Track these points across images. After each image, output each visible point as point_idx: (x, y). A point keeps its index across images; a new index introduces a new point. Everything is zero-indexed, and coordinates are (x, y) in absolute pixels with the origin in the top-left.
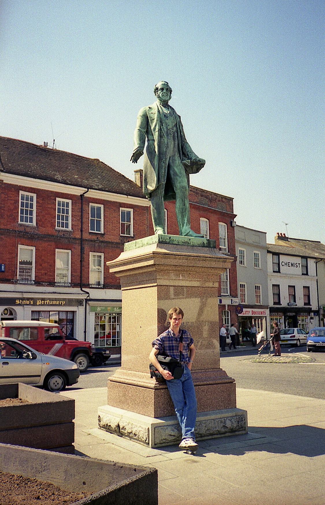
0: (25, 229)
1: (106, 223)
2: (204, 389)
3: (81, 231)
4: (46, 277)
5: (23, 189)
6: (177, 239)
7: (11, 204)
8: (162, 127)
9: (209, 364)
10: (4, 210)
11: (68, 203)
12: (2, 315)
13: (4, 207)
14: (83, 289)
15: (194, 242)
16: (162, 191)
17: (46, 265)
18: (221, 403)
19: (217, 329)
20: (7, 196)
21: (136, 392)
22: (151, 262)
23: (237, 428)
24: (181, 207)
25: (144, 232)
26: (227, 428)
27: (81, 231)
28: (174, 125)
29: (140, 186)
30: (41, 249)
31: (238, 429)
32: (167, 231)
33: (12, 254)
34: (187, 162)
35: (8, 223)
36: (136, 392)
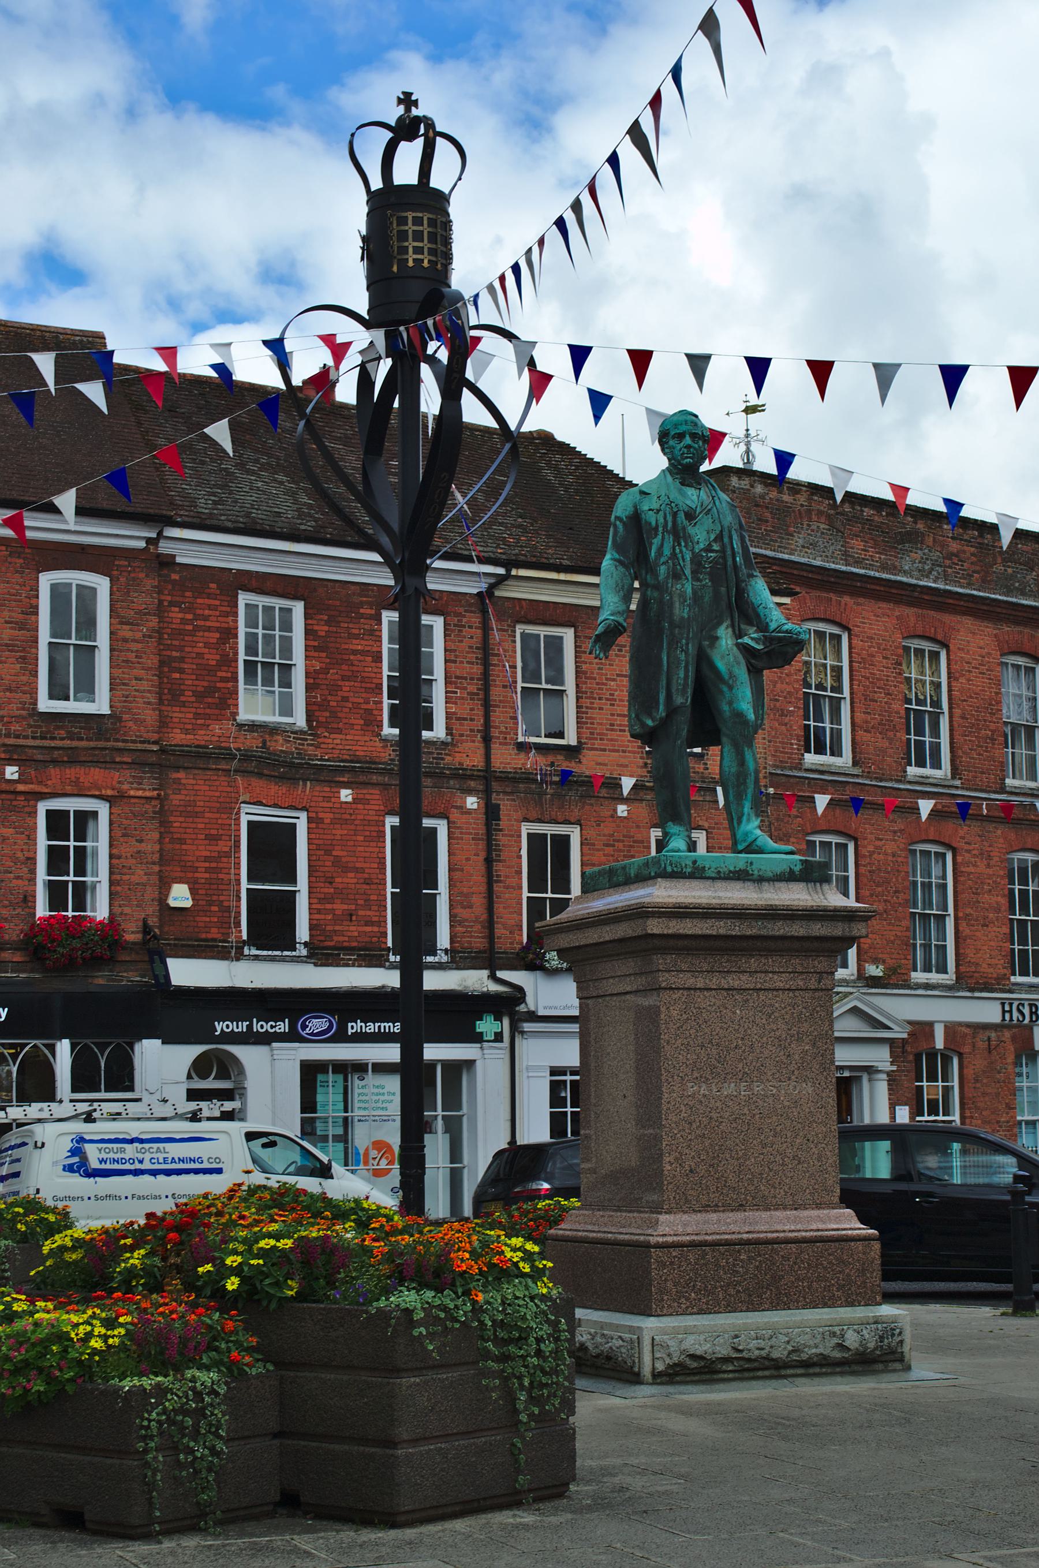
0: (264, 742)
1: (585, 702)
2: (790, 1254)
3: (487, 740)
4: (354, 930)
5: (254, 584)
6: (714, 865)
7: (207, 645)
8: (678, 550)
9: (808, 1191)
10: (181, 671)
12: (189, 1077)
13: (182, 659)
14: (501, 974)
15: (763, 868)
16: (683, 727)
17: (351, 878)
20: (190, 616)
23: (878, 1352)
26: (849, 1349)
27: (487, 740)
28: (713, 537)
30: (327, 817)
31: (879, 1356)
32: (852, 717)
34: (751, 638)
35: (199, 722)
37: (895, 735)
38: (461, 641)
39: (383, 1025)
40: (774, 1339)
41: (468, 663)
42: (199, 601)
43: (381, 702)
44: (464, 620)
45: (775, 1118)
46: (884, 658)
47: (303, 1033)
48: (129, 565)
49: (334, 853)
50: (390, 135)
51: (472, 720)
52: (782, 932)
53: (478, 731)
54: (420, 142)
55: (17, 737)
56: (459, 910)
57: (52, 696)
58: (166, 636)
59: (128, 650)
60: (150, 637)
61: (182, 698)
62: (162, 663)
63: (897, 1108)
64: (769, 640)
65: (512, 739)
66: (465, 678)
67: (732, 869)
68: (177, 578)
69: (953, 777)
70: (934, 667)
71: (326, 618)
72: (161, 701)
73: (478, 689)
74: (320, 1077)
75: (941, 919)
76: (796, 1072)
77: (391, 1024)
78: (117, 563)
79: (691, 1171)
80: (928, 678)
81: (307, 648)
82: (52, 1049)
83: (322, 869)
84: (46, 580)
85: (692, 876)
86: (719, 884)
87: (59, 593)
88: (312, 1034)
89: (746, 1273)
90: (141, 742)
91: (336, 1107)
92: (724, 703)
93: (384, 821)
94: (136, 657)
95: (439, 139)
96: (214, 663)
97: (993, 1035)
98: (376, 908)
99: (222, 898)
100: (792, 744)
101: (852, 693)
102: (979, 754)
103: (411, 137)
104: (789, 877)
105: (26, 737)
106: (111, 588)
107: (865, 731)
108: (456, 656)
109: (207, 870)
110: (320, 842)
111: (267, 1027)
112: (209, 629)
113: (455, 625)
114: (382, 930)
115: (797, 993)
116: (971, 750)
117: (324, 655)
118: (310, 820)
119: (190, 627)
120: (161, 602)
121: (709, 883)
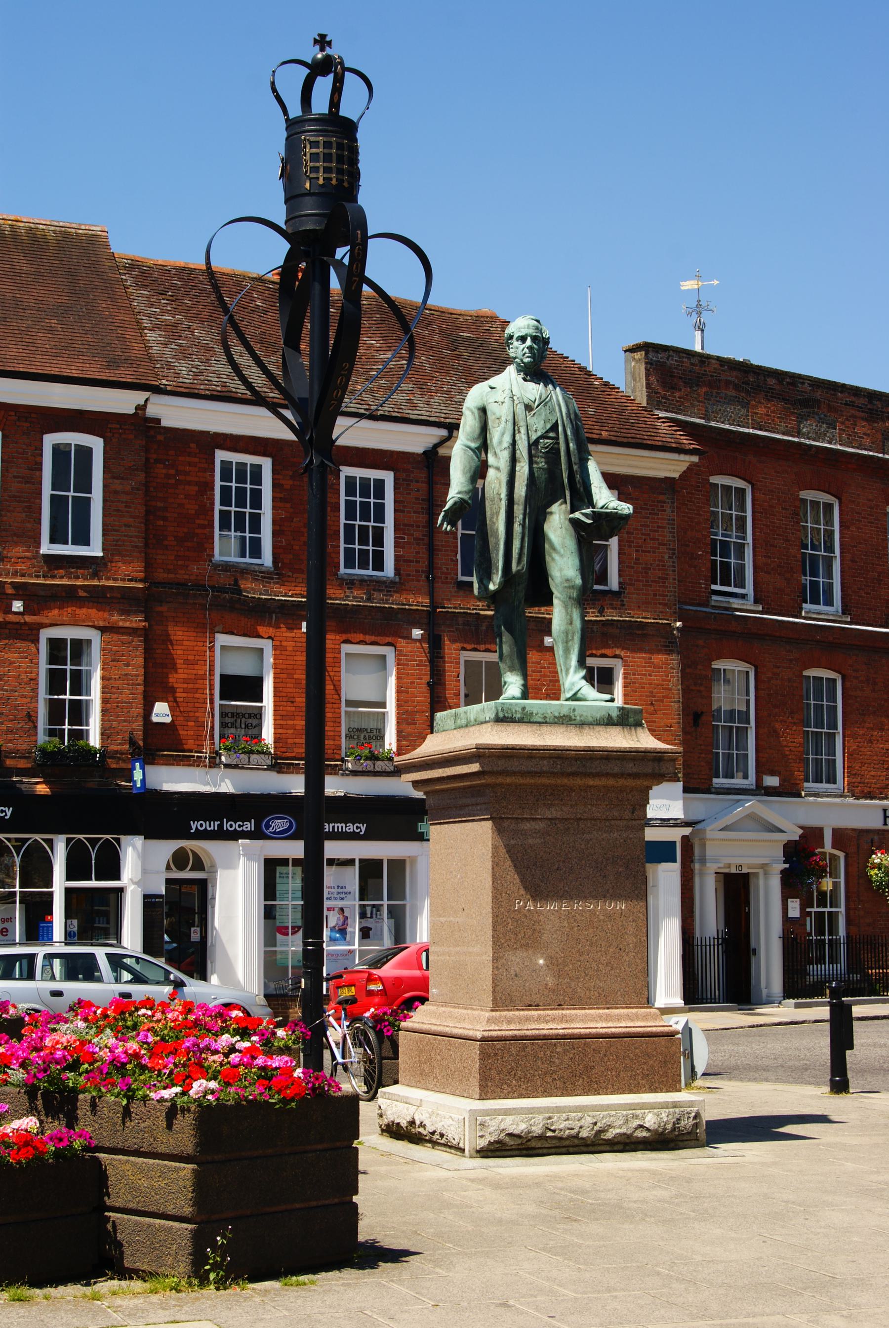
0: (236, 581)
6: (541, 712)
9: (619, 993)
10: (165, 519)
11: (380, 484)
12: (168, 868)
15: (585, 714)
18: (643, 1079)
19: (641, 915)
20: (172, 472)
21: (449, 1050)
22: (475, 767)
24: (563, 628)
25: (660, 574)
29: (645, 404)
33: (197, 667)
35: (180, 563)
36: (449, 1050)
37: (792, 576)
38: (409, 494)
39: (336, 825)
40: (583, 1121)
41: (415, 512)
42: (181, 458)
43: (339, 546)
44: (412, 475)
45: (591, 930)
46: (783, 509)
47: (267, 832)
48: (121, 428)
49: (296, 676)
50: (306, 71)
51: (417, 562)
52: (598, 770)
53: (423, 571)
54: (331, 77)
55: (23, 575)
56: (404, 726)
57: (53, 540)
58: (152, 489)
59: (119, 501)
60: (138, 489)
61: (166, 543)
62: (148, 512)
63: (789, 900)
64: (596, 516)
65: (452, 578)
66: (412, 526)
67: (557, 714)
68: (162, 439)
69: (843, 613)
70: (828, 518)
71: (291, 473)
72: (146, 545)
73: (423, 535)
74: (279, 869)
75: (831, 737)
76: (611, 891)
77: (343, 825)
78: (110, 426)
79: (516, 975)
80: (822, 527)
81: (274, 499)
82: (50, 842)
83: (284, 690)
84: (50, 440)
85: (520, 721)
86: (545, 729)
87: (60, 452)
88: (274, 833)
89: (561, 1063)
90: (130, 580)
91: (294, 896)
92: (556, 571)
93: (340, 649)
94: (126, 507)
95: (347, 74)
96: (193, 512)
97: (876, 838)
98: (332, 724)
99: (197, 714)
100: (701, 584)
101: (754, 540)
102: (867, 593)
103: (325, 74)
104: (608, 722)
105: (30, 576)
106: (105, 447)
107: (765, 573)
108: (404, 507)
109: (185, 691)
110: (284, 667)
111: (236, 826)
112: (189, 483)
113: (403, 480)
114: (336, 743)
115: (613, 822)
116: (860, 589)
117: (289, 505)
118: (275, 648)
119: (173, 481)
120: (147, 460)
121: (535, 727)
